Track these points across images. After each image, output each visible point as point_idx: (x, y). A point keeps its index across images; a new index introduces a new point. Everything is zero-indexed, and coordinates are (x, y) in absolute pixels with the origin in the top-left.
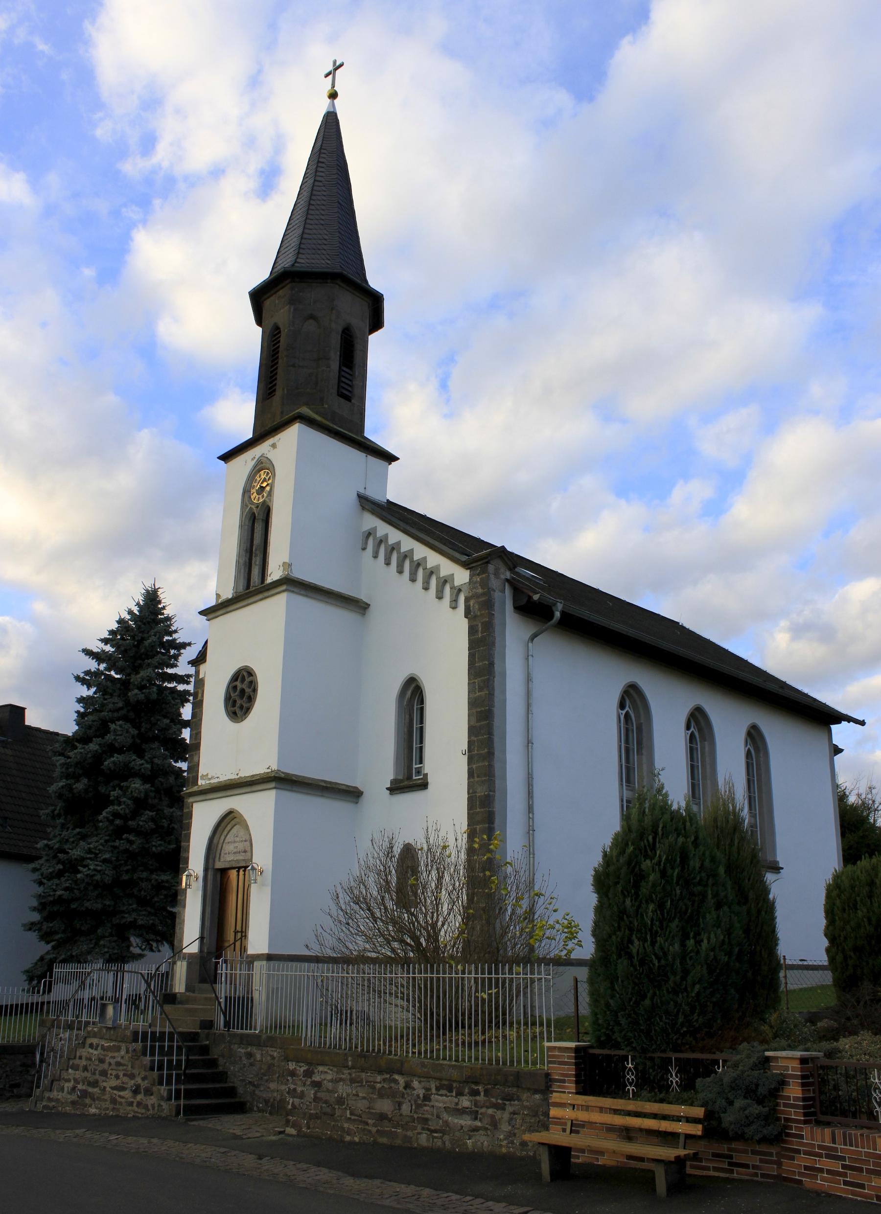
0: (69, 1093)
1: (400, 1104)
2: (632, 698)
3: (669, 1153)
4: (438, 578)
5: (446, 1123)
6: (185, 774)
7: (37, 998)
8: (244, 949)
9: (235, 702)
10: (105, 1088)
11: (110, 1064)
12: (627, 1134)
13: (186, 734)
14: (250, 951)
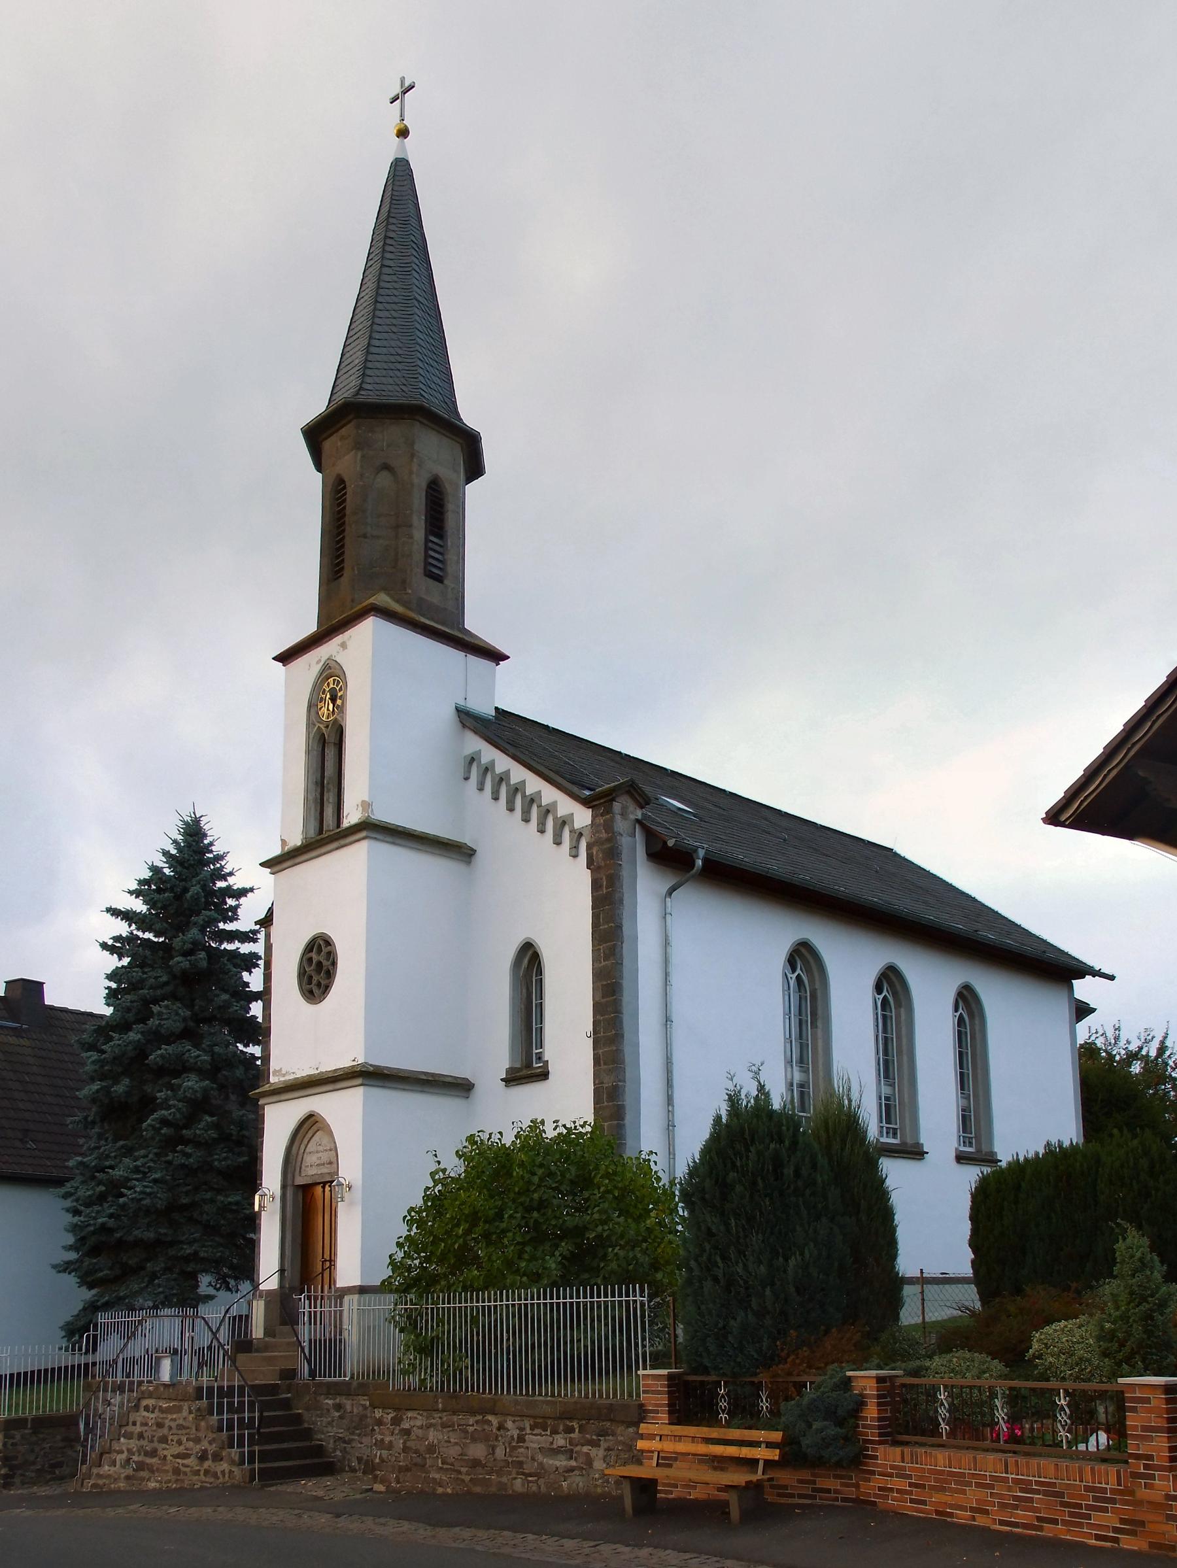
0: (123, 1467)
1: (494, 1448)
2: (803, 958)
3: (740, 1478)
4: (555, 819)
5: (541, 1464)
6: (259, 1063)
7: (79, 1359)
8: (332, 1281)
9: (311, 977)
10: (165, 1456)
11: (170, 1428)
12: (719, 1463)
13: (256, 1009)
14: (341, 1283)
